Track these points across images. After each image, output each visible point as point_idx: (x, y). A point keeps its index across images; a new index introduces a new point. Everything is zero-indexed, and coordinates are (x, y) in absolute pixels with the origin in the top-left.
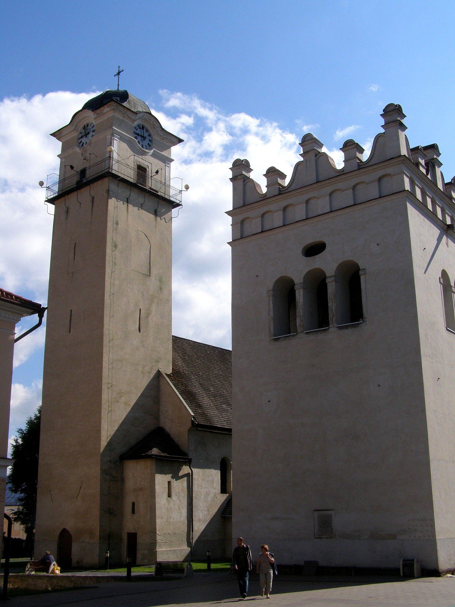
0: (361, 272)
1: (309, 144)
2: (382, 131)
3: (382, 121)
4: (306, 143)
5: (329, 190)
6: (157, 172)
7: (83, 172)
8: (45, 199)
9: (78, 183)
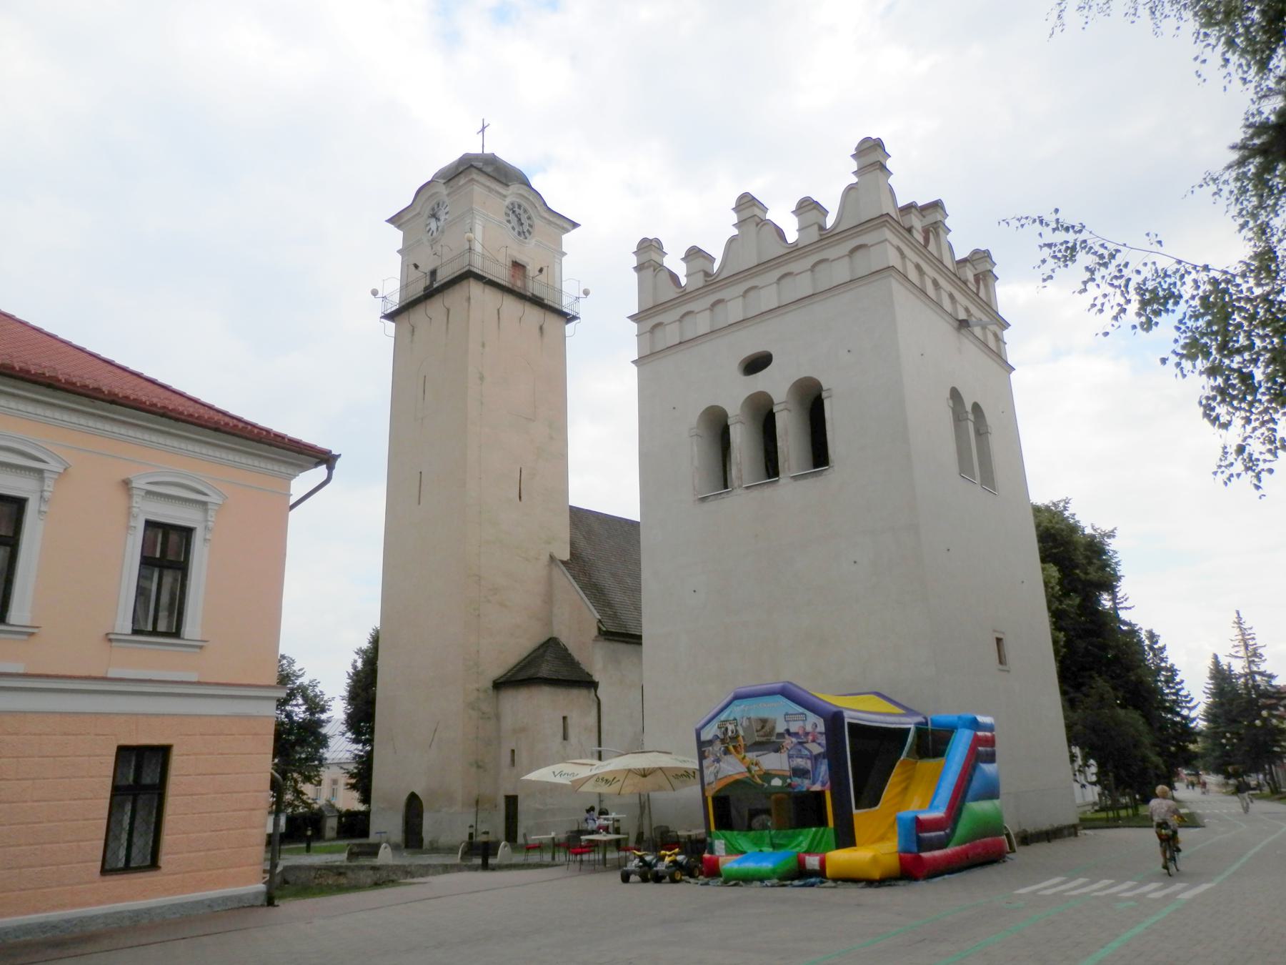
0: (824, 395)
1: (748, 207)
2: (854, 180)
3: (854, 165)
5: (777, 273)
6: (541, 270)
7: (433, 273)
9: (426, 289)
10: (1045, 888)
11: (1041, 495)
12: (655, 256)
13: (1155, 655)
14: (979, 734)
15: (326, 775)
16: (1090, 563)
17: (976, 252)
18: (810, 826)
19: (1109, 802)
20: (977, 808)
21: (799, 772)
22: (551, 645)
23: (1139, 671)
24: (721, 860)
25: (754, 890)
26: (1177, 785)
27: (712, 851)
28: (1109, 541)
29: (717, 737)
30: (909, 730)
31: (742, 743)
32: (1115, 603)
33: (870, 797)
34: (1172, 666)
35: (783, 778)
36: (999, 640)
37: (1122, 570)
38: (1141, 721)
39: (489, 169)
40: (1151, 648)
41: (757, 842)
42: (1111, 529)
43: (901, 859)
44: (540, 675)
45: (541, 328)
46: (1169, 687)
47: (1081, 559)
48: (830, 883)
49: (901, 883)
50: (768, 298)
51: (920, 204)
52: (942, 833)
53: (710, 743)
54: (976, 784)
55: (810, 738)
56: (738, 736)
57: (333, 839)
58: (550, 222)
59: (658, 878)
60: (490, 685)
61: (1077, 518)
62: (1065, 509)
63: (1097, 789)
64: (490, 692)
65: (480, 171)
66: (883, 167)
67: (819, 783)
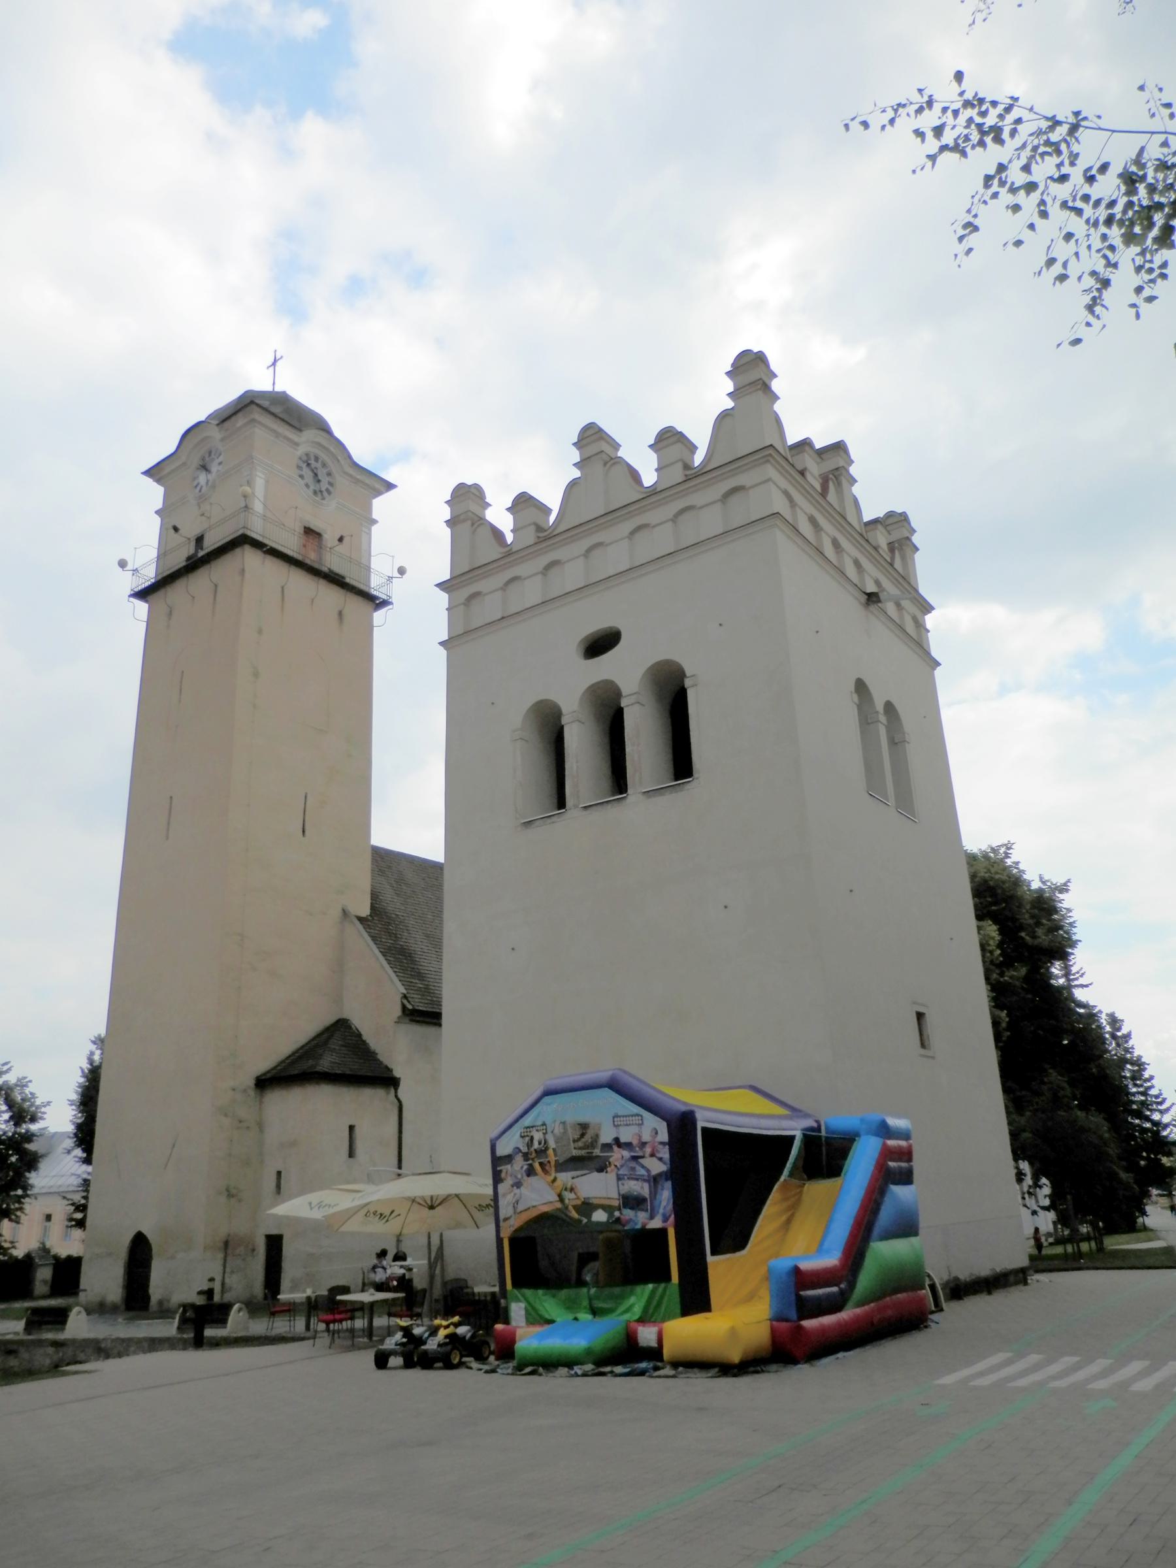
0: (688, 683)
1: (593, 442)
2: (729, 404)
4: (584, 442)
6: (341, 539)
7: (199, 540)
8: (129, 592)
9: (189, 558)
10: (981, 1374)
11: (976, 836)
12: (473, 507)
13: (1118, 1045)
14: (891, 1143)
15: (33, 1210)
16: (1038, 924)
17: (890, 514)
18: (645, 1281)
19: (1067, 1232)
20: (885, 1252)
21: (633, 1202)
22: (341, 1028)
23: (1101, 1062)
24: (519, 1333)
25: (557, 1383)
26: (1148, 1208)
27: (507, 1321)
28: (1061, 896)
29: (518, 1150)
30: (793, 1138)
31: (552, 1158)
32: (1069, 980)
33: (733, 1237)
34: (1139, 1057)
35: (608, 1209)
36: (920, 1016)
37: (1078, 933)
38: (1105, 1127)
39: (277, 410)
40: (1114, 1037)
41: (571, 1306)
42: (1063, 881)
43: (773, 1331)
44: (319, 1069)
45: (340, 613)
46: (1136, 1085)
47: (1026, 919)
48: (668, 1371)
49: (774, 1367)
50: (616, 557)
51: (818, 445)
52: (835, 1289)
53: (508, 1159)
54: (885, 1217)
55: (648, 1150)
56: (547, 1149)
57: (44, 1297)
58: (357, 481)
59: (426, 1362)
60: (251, 1082)
61: (1021, 867)
62: (1007, 855)
63: (1051, 1216)
64: (252, 1093)
65: (266, 413)
66: (766, 388)
67: (659, 1217)
